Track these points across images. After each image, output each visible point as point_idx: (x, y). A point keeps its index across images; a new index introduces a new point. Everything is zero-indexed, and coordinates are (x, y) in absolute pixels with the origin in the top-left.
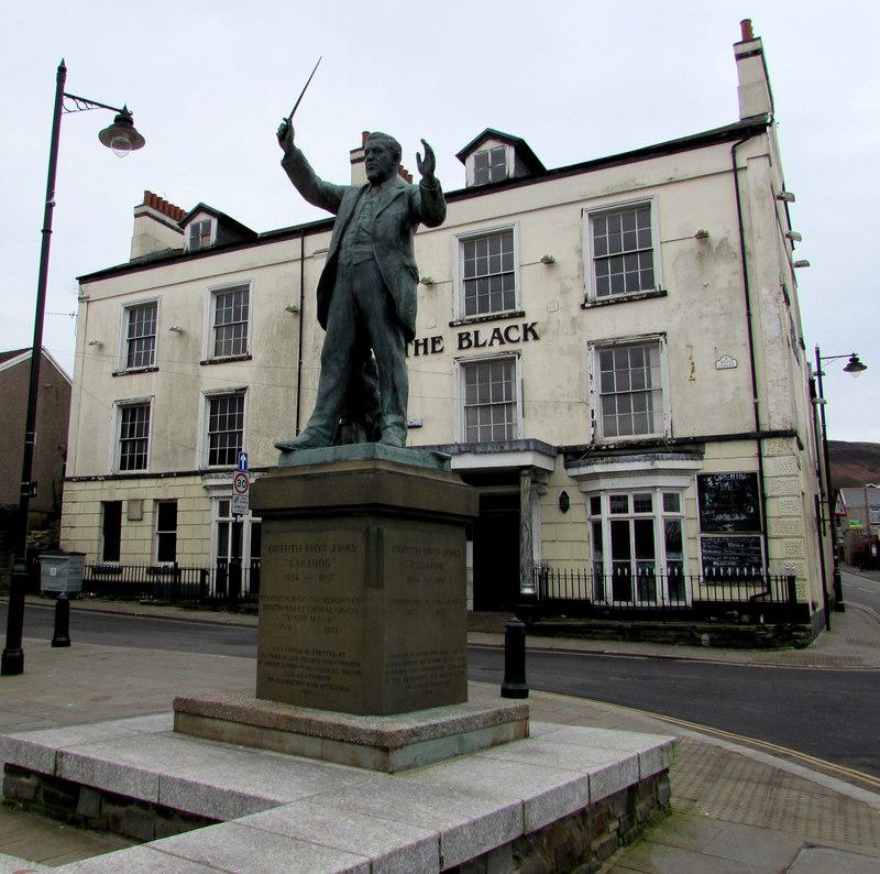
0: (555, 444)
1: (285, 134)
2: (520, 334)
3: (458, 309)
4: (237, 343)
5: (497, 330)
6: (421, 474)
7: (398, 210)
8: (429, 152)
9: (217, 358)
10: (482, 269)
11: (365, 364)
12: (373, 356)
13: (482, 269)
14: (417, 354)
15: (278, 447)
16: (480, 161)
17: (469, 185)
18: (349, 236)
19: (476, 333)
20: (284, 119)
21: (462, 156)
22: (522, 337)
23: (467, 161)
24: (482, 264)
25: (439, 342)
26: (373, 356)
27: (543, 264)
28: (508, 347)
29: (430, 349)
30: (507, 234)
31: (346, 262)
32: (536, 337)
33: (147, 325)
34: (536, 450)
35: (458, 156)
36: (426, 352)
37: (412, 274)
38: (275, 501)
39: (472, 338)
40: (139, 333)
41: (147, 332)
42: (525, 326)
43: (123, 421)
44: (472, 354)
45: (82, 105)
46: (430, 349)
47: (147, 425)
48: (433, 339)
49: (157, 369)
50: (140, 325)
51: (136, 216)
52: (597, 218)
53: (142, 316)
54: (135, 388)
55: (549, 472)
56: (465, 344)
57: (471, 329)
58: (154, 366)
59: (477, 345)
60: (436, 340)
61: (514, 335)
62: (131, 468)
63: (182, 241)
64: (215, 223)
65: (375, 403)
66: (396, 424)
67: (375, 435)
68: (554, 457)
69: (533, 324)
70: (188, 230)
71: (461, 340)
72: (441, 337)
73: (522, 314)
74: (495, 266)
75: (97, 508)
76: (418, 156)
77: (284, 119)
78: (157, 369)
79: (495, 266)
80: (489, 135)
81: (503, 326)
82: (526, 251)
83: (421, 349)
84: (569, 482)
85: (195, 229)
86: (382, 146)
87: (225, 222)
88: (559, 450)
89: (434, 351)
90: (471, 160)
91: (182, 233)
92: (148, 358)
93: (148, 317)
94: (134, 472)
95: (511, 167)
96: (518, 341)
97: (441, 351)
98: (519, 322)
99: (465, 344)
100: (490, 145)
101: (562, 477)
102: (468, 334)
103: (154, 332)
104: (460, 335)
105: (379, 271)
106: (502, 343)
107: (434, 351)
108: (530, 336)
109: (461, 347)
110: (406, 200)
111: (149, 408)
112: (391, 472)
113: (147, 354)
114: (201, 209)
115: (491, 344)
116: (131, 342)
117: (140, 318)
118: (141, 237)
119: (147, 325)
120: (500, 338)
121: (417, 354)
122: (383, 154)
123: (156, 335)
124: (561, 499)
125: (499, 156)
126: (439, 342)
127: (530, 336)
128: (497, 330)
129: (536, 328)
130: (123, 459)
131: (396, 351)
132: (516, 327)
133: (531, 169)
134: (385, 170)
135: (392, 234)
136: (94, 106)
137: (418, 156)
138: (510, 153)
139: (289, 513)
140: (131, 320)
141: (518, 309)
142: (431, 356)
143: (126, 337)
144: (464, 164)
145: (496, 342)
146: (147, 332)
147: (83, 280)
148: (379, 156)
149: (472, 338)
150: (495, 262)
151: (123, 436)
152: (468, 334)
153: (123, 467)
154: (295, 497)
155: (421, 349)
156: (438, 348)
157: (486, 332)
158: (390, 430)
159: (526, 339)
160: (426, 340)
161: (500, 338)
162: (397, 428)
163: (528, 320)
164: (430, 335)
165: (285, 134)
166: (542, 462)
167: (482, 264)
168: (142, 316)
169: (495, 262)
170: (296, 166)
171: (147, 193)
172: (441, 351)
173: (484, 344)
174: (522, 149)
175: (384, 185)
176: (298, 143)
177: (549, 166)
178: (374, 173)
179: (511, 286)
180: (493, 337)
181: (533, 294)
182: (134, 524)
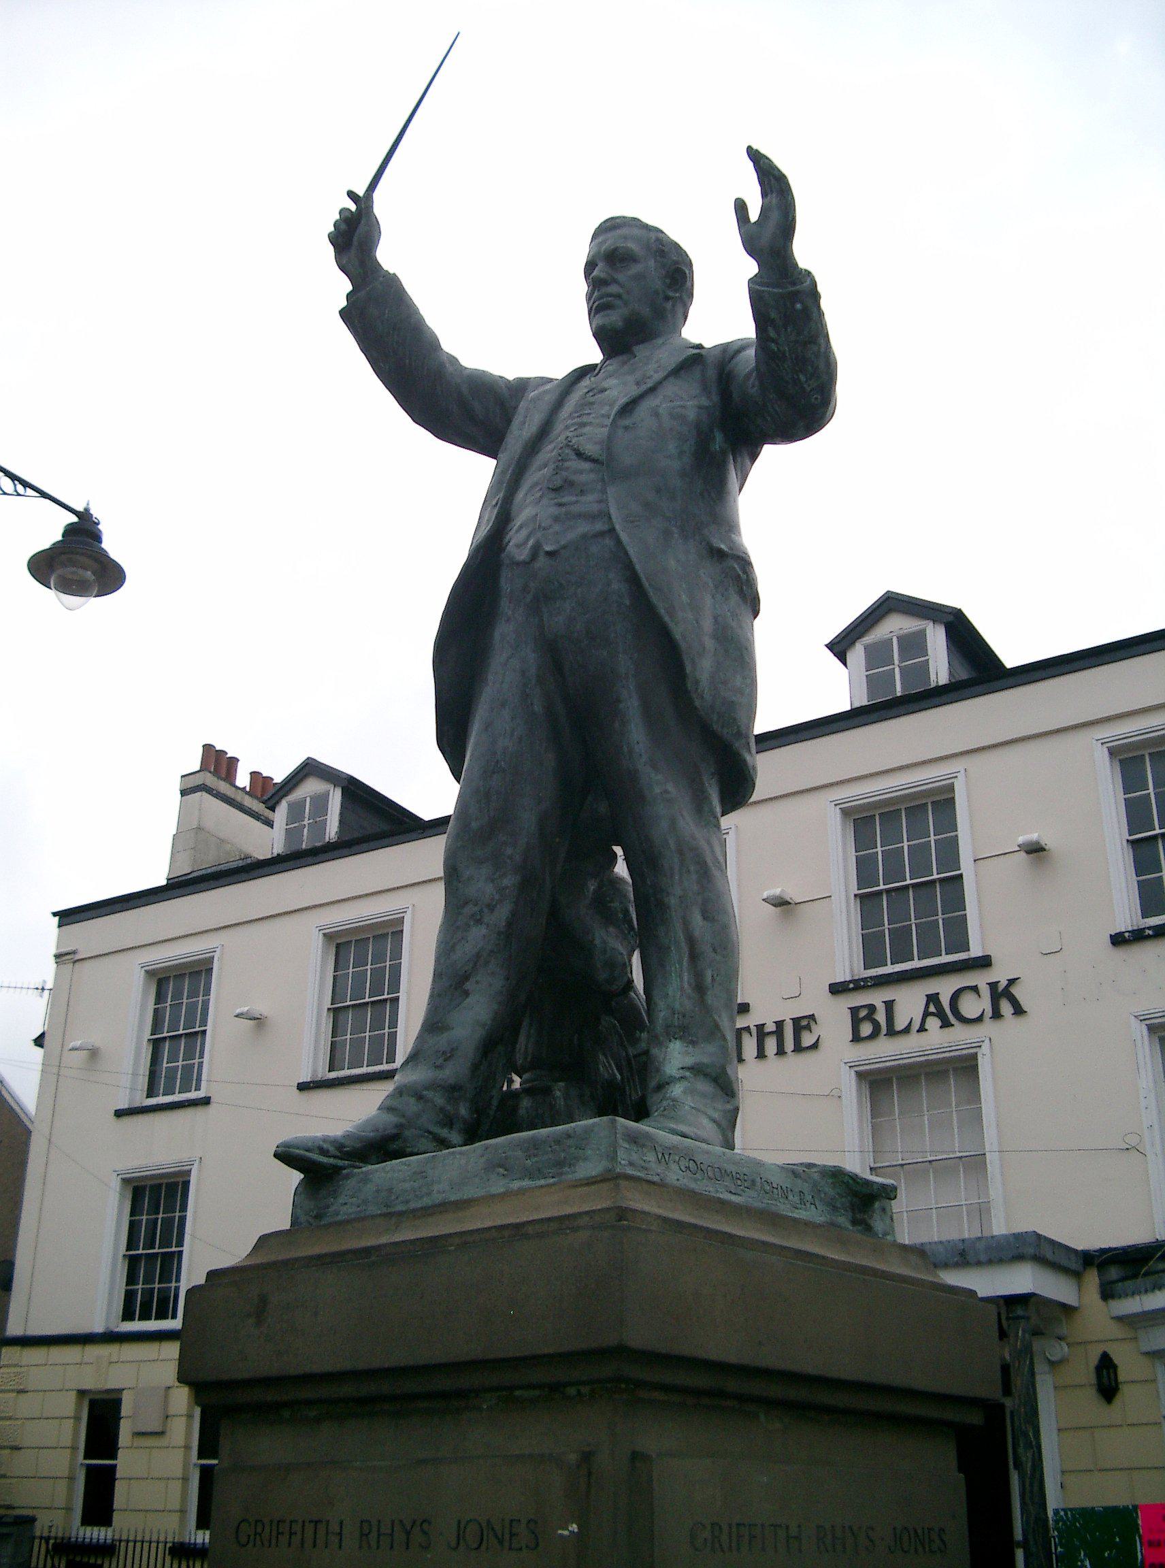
0: (1080, 1246)
1: (354, 236)
2: (985, 1004)
3: (846, 961)
4: (376, 1042)
5: (933, 999)
6: (794, 1243)
7: (687, 401)
8: (772, 180)
9: (333, 1075)
10: (895, 871)
11: (592, 886)
12: (621, 869)
13: (895, 871)
14: (761, 1055)
15: (286, 1156)
16: (877, 655)
17: (857, 705)
18: (537, 474)
19: (889, 1005)
20: (351, 195)
21: (839, 648)
22: (989, 1012)
23: (850, 657)
24: (893, 858)
25: (808, 1028)
26: (621, 869)
27: (1023, 854)
28: (959, 1036)
29: (789, 1044)
30: (941, 802)
31: (523, 555)
32: (1019, 1011)
33: (192, 1008)
34: (1040, 1260)
35: (831, 646)
36: (781, 1052)
37: (741, 593)
38: (252, 1354)
39: (881, 1017)
40: (174, 1026)
41: (190, 1023)
42: (993, 986)
43: (133, 1213)
44: (884, 1051)
45: (20, 488)
46: (789, 1044)
47: (183, 1220)
48: (796, 1021)
49: (206, 1101)
50: (176, 1007)
51: (184, 793)
52: (1128, 760)
53: (179, 991)
54: (159, 1145)
55: (1067, 1310)
56: (866, 1029)
57: (877, 998)
58: (201, 1094)
59: (892, 1032)
60: (802, 1024)
61: (970, 1006)
62: (145, 1316)
63: (267, 840)
64: (336, 799)
65: (632, 1022)
66: (697, 1070)
67: (631, 1096)
68: (1077, 1275)
69: (1012, 982)
70: (280, 815)
71: (856, 1023)
72: (812, 1017)
73: (984, 962)
74: (921, 865)
75: (68, 1405)
76: (741, 208)
77: (351, 195)
78: (206, 1101)
79: (921, 865)
80: (891, 604)
81: (945, 987)
82: (983, 832)
83: (771, 1045)
84: (1116, 1331)
85: (296, 812)
86: (631, 245)
87: (358, 795)
88: (1090, 1259)
89: (798, 1048)
90: (857, 654)
91: (269, 823)
92: (191, 1078)
93: (193, 993)
94: (153, 1325)
95: (939, 664)
96: (979, 1019)
97: (815, 1046)
98: (980, 979)
99: (866, 1029)
100: (895, 626)
101: (1097, 1317)
102: (872, 1008)
103: (204, 1022)
104: (854, 1011)
105: (629, 567)
106: (946, 1024)
107: (798, 1048)
108: (1006, 1008)
109: (856, 1038)
110: (712, 373)
111: (186, 1184)
112: (680, 1226)
113: (188, 1070)
114: (309, 769)
115: (922, 1029)
116: (156, 1044)
117: (178, 995)
118: (189, 835)
119: (192, 1008)
120: (940, 1014)
121: (761, 1055)
122: (635, 269)
123: (209, 1028)
124: (1099, 1369)
125: (914, 645)
126: (808, 1028)
127: (1006, 1008)
128: (933, 999)
129: (1015, 990)
130: (129, 1297)
131: (688, 824)
132: (975, 989)
133: (979, 668)
134: (646, 311)
135: (673, 459)
136: (30, 492)
137: (741, 208)
138: (937, 639)
139: (347, 1390)
140: (160, 998)
141: (975, 951)
142: (792, 1060)
143: (147, 1035)
144: (845, 664)
145: (933, 1023)
146: (190, 1023)
147: (67, 917)
148: (634, 278)
149: (881, 1017)
150: (919, 853)
151: (131, 1244)
152: (872, 1008)
153: (128, 1315)
154: (322, 1333)
155: (771, 1045)
156: (807, 1040)
157: (909, 1002)
158: (677, 1090)
159: (997, 1015)
160: (780, 1024)
161: (940, 1014)
162: (704, 1086)
163: (999, 974)
164: (788, 1013)
165: (354, 236)
166: (1055, 1288)
167: (893, 858)
168: (179, 991)
169: (919, 853)
170: (385, 326)
171: (208, 748)
172: (815, 1046)
173: (907, 1030)
174: (959, 629)
175: (641, 351)
176: (388, 256)
177: (1011, 658)
178: (614, 318)
179: (956, 900)
180: (926, 1014)
181: (995, 915)
182: (150, 1442)
